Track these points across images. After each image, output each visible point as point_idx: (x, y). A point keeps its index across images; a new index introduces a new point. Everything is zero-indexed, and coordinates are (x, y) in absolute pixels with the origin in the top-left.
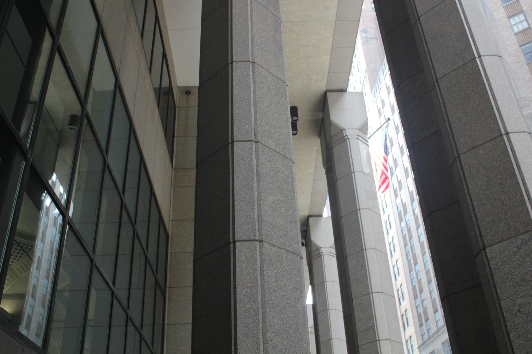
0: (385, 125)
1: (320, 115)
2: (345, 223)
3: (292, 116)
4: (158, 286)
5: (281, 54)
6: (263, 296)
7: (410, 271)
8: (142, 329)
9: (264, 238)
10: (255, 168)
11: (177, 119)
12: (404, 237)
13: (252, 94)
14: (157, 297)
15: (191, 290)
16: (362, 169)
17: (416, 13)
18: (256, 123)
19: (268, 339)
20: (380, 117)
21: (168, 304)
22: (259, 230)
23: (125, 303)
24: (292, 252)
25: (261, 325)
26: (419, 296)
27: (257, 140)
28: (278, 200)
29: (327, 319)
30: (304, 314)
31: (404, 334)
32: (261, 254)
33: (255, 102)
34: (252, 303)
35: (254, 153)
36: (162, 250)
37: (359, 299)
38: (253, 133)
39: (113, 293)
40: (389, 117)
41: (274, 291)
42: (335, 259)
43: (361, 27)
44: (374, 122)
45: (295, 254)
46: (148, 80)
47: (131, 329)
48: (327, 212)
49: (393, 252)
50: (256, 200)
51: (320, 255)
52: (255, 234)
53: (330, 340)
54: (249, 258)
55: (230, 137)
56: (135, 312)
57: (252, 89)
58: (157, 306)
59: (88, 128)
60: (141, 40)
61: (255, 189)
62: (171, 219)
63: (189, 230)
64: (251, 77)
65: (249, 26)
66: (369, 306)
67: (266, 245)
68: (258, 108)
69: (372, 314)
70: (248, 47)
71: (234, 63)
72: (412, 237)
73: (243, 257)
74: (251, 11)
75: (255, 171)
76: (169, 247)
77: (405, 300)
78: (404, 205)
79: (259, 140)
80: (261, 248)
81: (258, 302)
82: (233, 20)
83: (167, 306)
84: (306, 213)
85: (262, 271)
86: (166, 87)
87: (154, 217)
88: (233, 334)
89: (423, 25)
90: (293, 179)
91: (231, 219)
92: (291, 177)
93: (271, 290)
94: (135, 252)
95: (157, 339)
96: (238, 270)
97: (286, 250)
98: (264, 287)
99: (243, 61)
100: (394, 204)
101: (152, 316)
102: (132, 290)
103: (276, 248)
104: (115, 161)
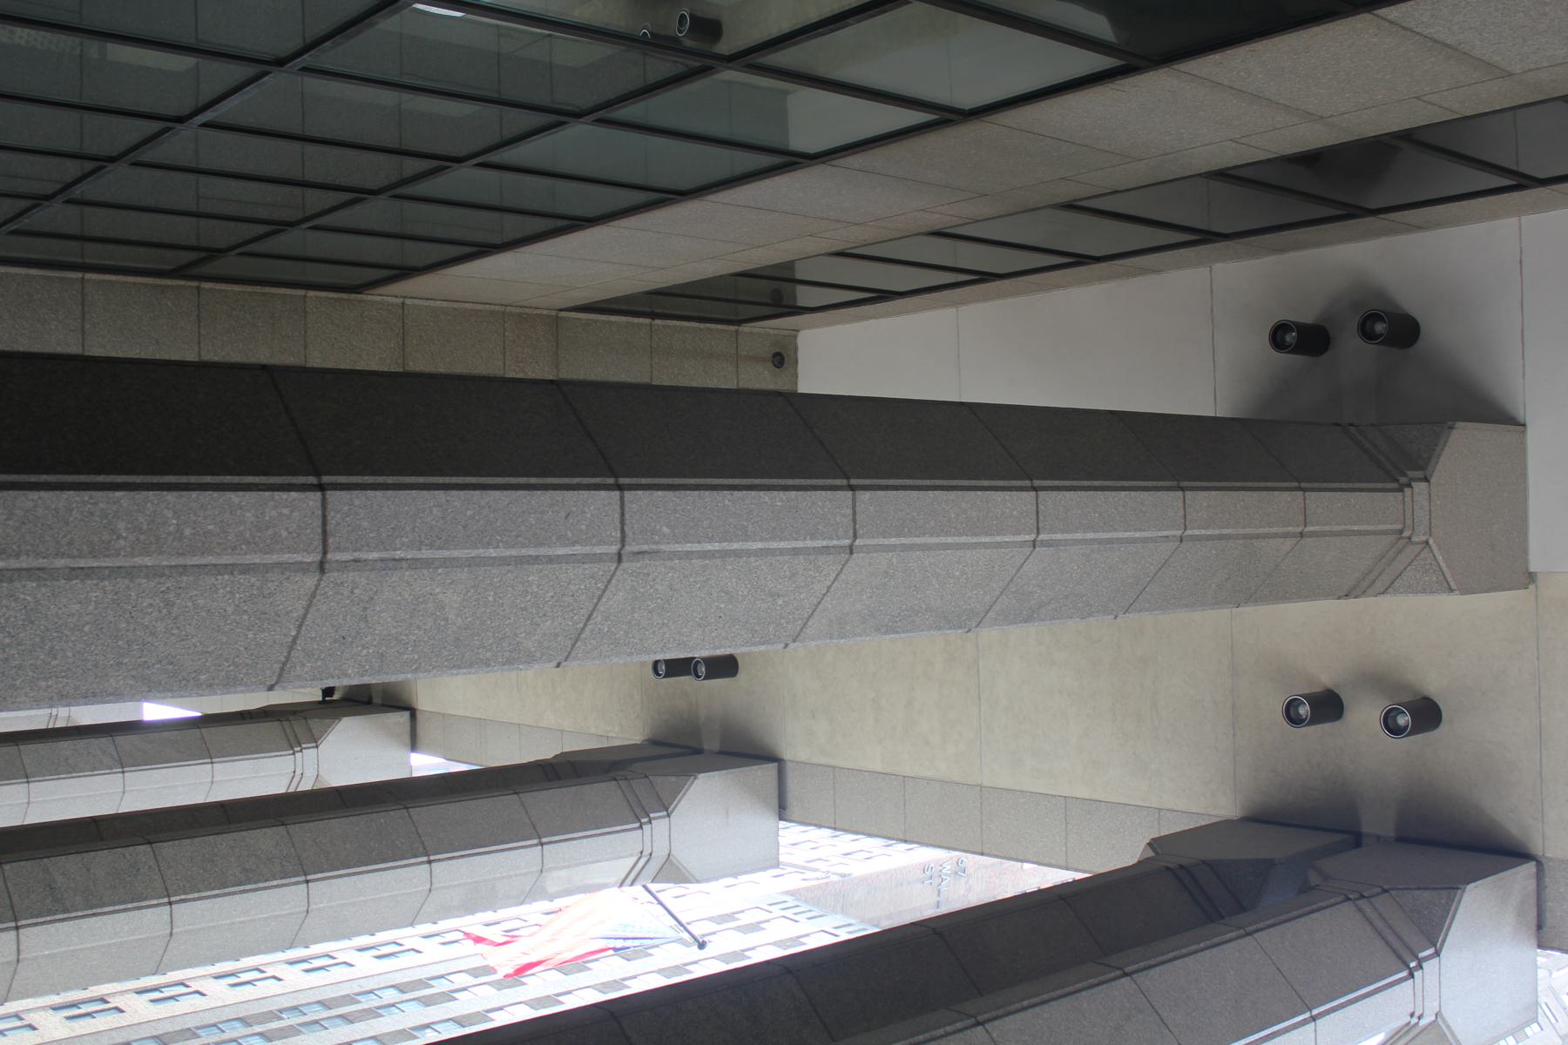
0: (686, 936)
1: (711, 744)
2: (389, 819)
3: (668, 663)
4: (203, 254)
5: (878, 630)
6: (155, 572)
7: (244, 1021)
8: (67, 202)
9: (332, 576)
10: (543, 551)
11: (702, 326)
12: (350, 999)
13: (760, 545)
14: (170, 254)
15: (191, 356)
16: (551, 869)
17: (994, 1014)
18: (673, 555)
19: (17, 585)
20: (710, 919)
21: (146, 285)
22: (355, 561)
23: (148, 155)
24: (288, 658)
25: (60, 563)
26: (249, 1031)
27: (624, 558)
28: (446, 620)
29: (94, 767)
30: (94, 695)
31: (43, 1008)
32: (283, 567)
33: (737, 554)
34: (132, 538)
35: (587, 549)
36: (315, 273)
37: (152, 863)
38: (645, 547)
39: (180, 120)
40: (709, 947)
41: (168, 604)
42: (282, 790)
43: (970, 860)
44: (695, 902)
45: (282, 669)
46: (812, 246)
47: (72, 169)
48: (425, 764)
49: (306, 966)
50: (446, 553)
51: (293, 744)
52: (345, 550)
53: (27, 777)
54: (270, 532)
55: (634, 481)
56: (118, 182)
57: (774, 545)
58: (141, 250)
59: (680, 69)
60: (925, 230)
61: (480, 552)
62: (408, 301)
63: (374, 355)
64: (809, 543)
65: (956, 539)
66: (128, 894)
67: (310, 581)
68: (718, 561)
69: (104, 905)
70: (897, 536)
71: (850, 494)
72: (352, 1022)
73: (274, 513)
74: (998, 545)
75: (532, 552)
76: (324, 294)
77: (68, 1023)
78: (448, 996)
79: (624, 565)
80: (302, 568)
81: (133, 556)
82: (972, 493)
83: (139, 280)
84: (423, 703)
85: (230, 569)
86: (795, 298)
87: (416, 253)
88: (33, 478)
89: (961, 1035)
90: (509, 662)
91: (390, 480)
92: (516, 657)
93: (171, 596)
94: (309, 191)
95: (38, 249)
96: (234, 497)
97: (294, 641)
98: (181, 574)
99: (854, 521)
100: (453, 967)
101: (112, 235)
102: (191, 177)
103: (302, 612)
104: (576, 145)
